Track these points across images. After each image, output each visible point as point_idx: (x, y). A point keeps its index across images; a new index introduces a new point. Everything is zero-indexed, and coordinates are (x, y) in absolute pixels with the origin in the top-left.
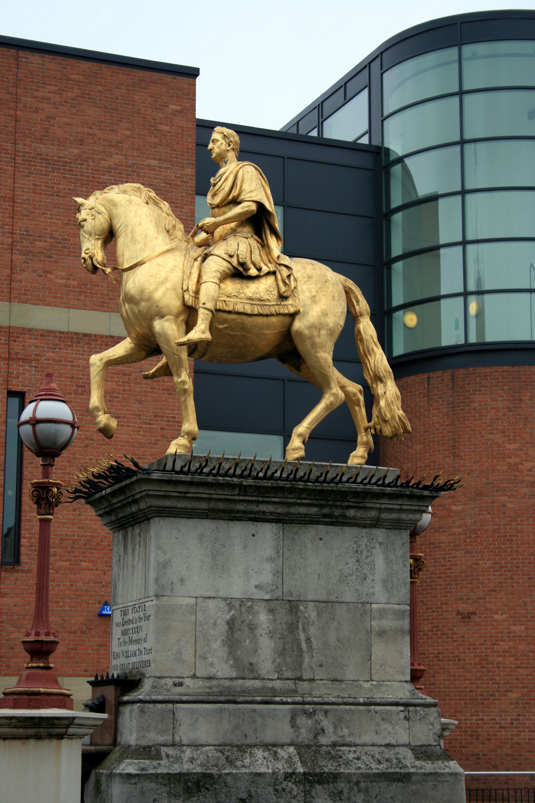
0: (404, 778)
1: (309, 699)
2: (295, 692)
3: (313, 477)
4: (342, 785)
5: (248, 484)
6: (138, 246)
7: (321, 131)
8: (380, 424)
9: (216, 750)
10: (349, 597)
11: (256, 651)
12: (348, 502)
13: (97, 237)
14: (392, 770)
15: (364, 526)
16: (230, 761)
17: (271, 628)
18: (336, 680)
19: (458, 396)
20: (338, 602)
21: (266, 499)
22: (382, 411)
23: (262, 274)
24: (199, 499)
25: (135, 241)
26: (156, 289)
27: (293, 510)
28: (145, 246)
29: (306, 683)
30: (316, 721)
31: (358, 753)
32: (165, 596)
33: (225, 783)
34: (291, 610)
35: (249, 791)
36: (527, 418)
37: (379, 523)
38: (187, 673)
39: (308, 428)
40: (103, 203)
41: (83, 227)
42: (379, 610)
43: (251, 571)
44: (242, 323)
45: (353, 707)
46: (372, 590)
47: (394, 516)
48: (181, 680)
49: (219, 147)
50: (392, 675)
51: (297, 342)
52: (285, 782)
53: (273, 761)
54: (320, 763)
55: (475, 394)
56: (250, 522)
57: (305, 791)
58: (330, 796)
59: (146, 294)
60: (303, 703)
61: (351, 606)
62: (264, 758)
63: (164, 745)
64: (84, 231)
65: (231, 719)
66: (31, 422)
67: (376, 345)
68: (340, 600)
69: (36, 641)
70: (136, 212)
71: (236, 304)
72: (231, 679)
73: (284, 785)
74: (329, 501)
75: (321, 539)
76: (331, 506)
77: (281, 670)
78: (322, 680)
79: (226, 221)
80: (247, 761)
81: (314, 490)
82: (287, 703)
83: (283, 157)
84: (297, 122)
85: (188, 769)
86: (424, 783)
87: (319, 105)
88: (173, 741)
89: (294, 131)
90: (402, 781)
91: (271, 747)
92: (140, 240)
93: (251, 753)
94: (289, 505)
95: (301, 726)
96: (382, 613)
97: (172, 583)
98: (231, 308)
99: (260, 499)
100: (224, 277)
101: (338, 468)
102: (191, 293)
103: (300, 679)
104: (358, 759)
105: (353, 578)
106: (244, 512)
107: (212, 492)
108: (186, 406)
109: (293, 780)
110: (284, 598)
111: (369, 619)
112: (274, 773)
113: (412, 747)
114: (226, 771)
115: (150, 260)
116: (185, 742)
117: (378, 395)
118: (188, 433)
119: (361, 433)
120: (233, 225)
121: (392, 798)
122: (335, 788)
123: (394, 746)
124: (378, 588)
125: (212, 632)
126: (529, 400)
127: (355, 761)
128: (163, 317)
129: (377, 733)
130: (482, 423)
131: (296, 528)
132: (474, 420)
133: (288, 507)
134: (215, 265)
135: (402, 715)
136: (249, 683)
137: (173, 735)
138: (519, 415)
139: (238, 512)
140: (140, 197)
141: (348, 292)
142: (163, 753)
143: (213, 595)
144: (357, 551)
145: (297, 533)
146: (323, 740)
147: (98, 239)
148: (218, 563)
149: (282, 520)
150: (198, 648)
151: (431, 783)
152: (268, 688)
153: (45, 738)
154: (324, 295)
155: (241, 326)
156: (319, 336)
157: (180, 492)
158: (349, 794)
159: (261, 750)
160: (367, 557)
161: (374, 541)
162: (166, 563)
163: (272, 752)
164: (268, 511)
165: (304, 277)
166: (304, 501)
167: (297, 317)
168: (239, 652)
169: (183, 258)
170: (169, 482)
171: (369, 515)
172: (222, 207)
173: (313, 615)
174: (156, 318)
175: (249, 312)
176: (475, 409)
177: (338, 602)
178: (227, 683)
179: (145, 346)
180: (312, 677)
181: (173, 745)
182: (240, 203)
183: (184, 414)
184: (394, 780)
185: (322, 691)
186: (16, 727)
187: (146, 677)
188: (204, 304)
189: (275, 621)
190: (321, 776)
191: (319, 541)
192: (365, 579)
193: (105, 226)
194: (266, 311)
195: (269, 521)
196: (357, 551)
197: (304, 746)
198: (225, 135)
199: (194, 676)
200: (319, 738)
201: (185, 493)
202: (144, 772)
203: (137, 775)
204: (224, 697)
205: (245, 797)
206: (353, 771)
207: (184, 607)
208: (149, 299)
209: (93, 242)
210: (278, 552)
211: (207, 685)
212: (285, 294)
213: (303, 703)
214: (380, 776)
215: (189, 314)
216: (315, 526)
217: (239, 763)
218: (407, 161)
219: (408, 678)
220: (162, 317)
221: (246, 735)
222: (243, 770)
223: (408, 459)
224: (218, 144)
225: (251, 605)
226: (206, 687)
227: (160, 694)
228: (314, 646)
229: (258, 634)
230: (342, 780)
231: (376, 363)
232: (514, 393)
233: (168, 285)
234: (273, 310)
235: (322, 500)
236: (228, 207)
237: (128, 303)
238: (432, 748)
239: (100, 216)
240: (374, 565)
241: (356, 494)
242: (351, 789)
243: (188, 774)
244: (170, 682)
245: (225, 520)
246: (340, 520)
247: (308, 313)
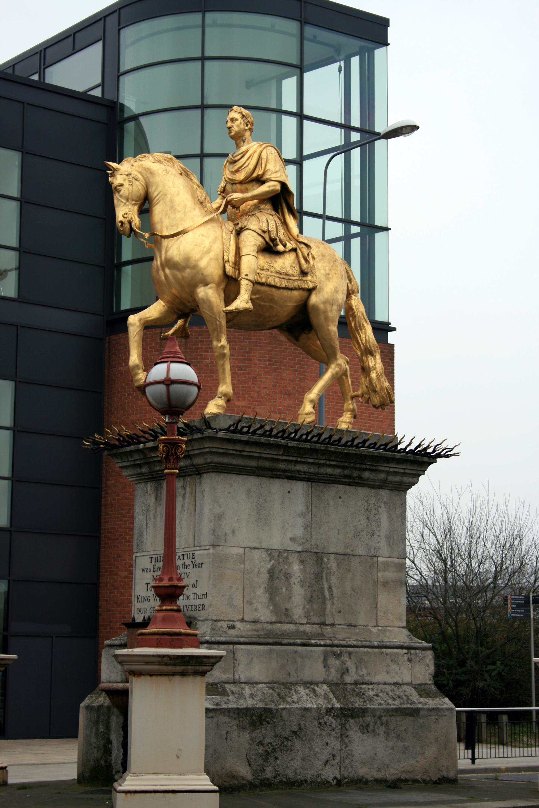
0: (414, 713)
1: (336, 642)
3: (343, 441)
4: (369, 719)
5: (292, 445)
6: (179, 215)
7: (42, 75)
8: (369, 394)
9: (268, 687)
10: (361, 551)
11: (291, 598)
12: (365, 464)
13: (133, 202)
14: (405, 706)
15: (373, 487)
16: (282, 698)
17: (302, 576)
18: (351, 625)
19: (191, 352)
20: (353, 555)
21: (303, 460)
22: (374, 382)
23: (287, 250)
24: (250, 457)
25: (174, 210)
26: (201, 258)
27: (322, 470)
28: (185, 215)
29: (329, 627)
30: (343, 662)
31: (375, 691)
32: (220, 546)
33: (281, 717)
34: (317, 561)
35: (300, 724)
36: (256, 378)
37: (386, 484)
38: (237, 617)
39: (318, 394)
40: (139, 170)
41: (119, 192)
42: (383, 562)
43: (287, 525)
44: (272, 295)
45: (369, 650)
46: (378, 545)
47: (398, 479)
48: (233, 623)
49: (238, 126)
50: (393, 621)
51: (312, 316)
52: (327, 717)
53: (314, 697)
54: (350, 700)
55: (207, 352)
56: (286, 480)
57: (341, 724)
58: (360, 729)
59: (193, 262)
60: (332, 646)
61: (363, 559)
62: (307, 694)
63: (227, 683)
64: (121, 196)
65: (279, 659)
66: (166, 383)
67: (366, 321)
68: (355, 553)
69: (171, 586)
70: (173, 182)
71: (267, 277)
72: (271, 623)
73: (325, 719)
74: (351, 463)
75: (340, 498)
76: (352, 467)
77: (310, 616)
78: (340, 625)
79: (253, 198)
80: (295, 697)
81: (341, 453)
82: (320, 645)
83: (23, 103)
85: (252, 704)
86: (428, 718)
87: (41, 51)
88: (234, 679)
89: (10, 71)
90: (413, 716)
92: (180, 209)
93: (295, 690)
94: (320, 465)
95: (331, 666)
96: (386, 565)
97: (226, 534)
98: (264, 280)
99: (299, 459)
101: (353, 433)
102: (231, 263)
103: (324, 624)
104: (377, 696)
105: (364, 533)
106: (284, 471)
107: (262, 452)
108: (224, 370)
109: (332, 714)
110: (312, 551)
111: (375, 571)
112: (318, 708)
113: (414, 686)
114: (282, 706)
115: (192, 230)
116: (243, 680)
117: (369, 367)
118: (225, 395)
119: (348, 401)
120: (255, 201)
121: (405, 730)
122: (364, 721)
123: (400, 685)
124: (383, 543)
125: (256, 579)
126: (259, 360)
127: (376, 697)
128: (207, 285)
129: (388, 673)
130: (213, 380)
131: (321, 487)
132: (205, 376)
133: (319, 467)
135: (406, 657)
137: (234, 674)
138: (249, 374)
139: (279, 470)
140: (174, 168)
142: (228, 690)
143: (257, 546)
144: (367, 510)
145: (322, 492)
146: (348, 679)
147: (135, 204)
148: (261, 516)
149: (312, 479)
150: (246, 595)
151: (434, 717)
152: (301, 632)
153: (189, 675)
154: (335, 273)
155: (270, 297)
156: (331, 311)
157: (236, 450)
158: (374, 727)
159: (302, 688)
160: (375, 515)
161: (380, 500)
162: (221, 516)
163: (311, 689)
164: (303, 470)
165: (319, 256)
166: (332, 463)
167: (314, 292)
168: (277, 599)
169: (220, 229)
170: (229, 441)
171: (379, 477)
172: (245, 183)
173: (333, 565)
174: (201, 285)
175: (279, 285)
176: (207, 366)
177: (353, 555)
178: (269, 627)
179: (179, 310)
180: (333, 622)
181: (234, 683)
182: (264, 182)
183: (221, 376)
184: (407, 715)
185: (342, 635)
186: (166, 664)
187: (198, 620)
188: (247, 275)
189: (305, 570)
190: (353, 711)
191: (338, 499)
192: (373, 535)
193: (142, 192)
194: (290, 285)
195: (301, 479)
196: (367, 510)
197: (333, 684)
198: (243, 115)
199: (242, 620)
200: (345, 677)
201: (240, 451)
202: (218, 707)
203: (213, 709)
204: (270, 640)
205: (296, 730)
206: (377, 707)
207: (235, 556)
208: (195, 267)
209: (130, 207)
210: (308, 508)
211: (254, 628)
212: (306, 271)
213: (332, 646)
214: (398, 711)
215: (230, 284)
216: (336, 485)
218: (142, 120)
219: (404, 624)
220: (207, 285)
221: (289, 674)
222: (295, 706)
223: (137, 410)
224: (237, 123)
225: (287, 556)
226: (253, 630)
227: (221, 636)
228: (335, 595)
229: (292, 583)
230: (369, 715)
231: (367, 338)
232: (244, 352)
233: (212, 254)
234: (296, 284)
235: (346, 462)
236: (251, 184)
237: (170, 268)
238: (429, 687)
239: (137, 183)
240: (380, 522)
241: (373, 458)
242: (375, 723)
243: (252, 709)
245: (267, 477)
246: (356, 481)
247: (323, 289)
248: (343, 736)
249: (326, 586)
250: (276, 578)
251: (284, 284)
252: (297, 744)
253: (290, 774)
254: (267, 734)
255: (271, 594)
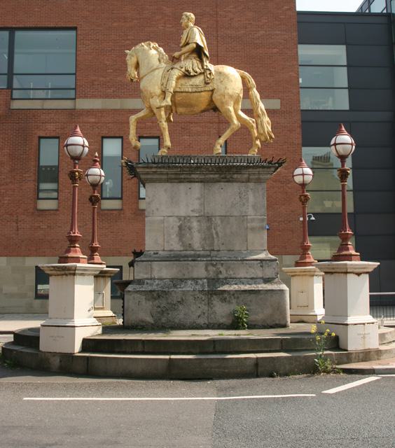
2: (209, 256)
7: (370, 11)
11: (192, 238)
34: (208, 220)
72: (181, 251)
84: (361, 8)
89: (360, 11)
91: (195, 280)
96: (253, 220)
100: (178, 78)
103: (214, 250)
131: (210, 184)
134: (177, 73)
135: (259, 265)
136: (188, 252)
141: (243, 78)
173: (219, 222)
178: (179, 252)
195: (197, 182)
199: (164, 250)
204: (174, 258)
217: (179, 286)
244: (152, 253)
248: (209, 304)
249: (214, 232)
250: (182, 230)
251: (194, 90)
252: (181, 307)
253: (177, 321)
254: (163, 303)
255: (180, 237)
